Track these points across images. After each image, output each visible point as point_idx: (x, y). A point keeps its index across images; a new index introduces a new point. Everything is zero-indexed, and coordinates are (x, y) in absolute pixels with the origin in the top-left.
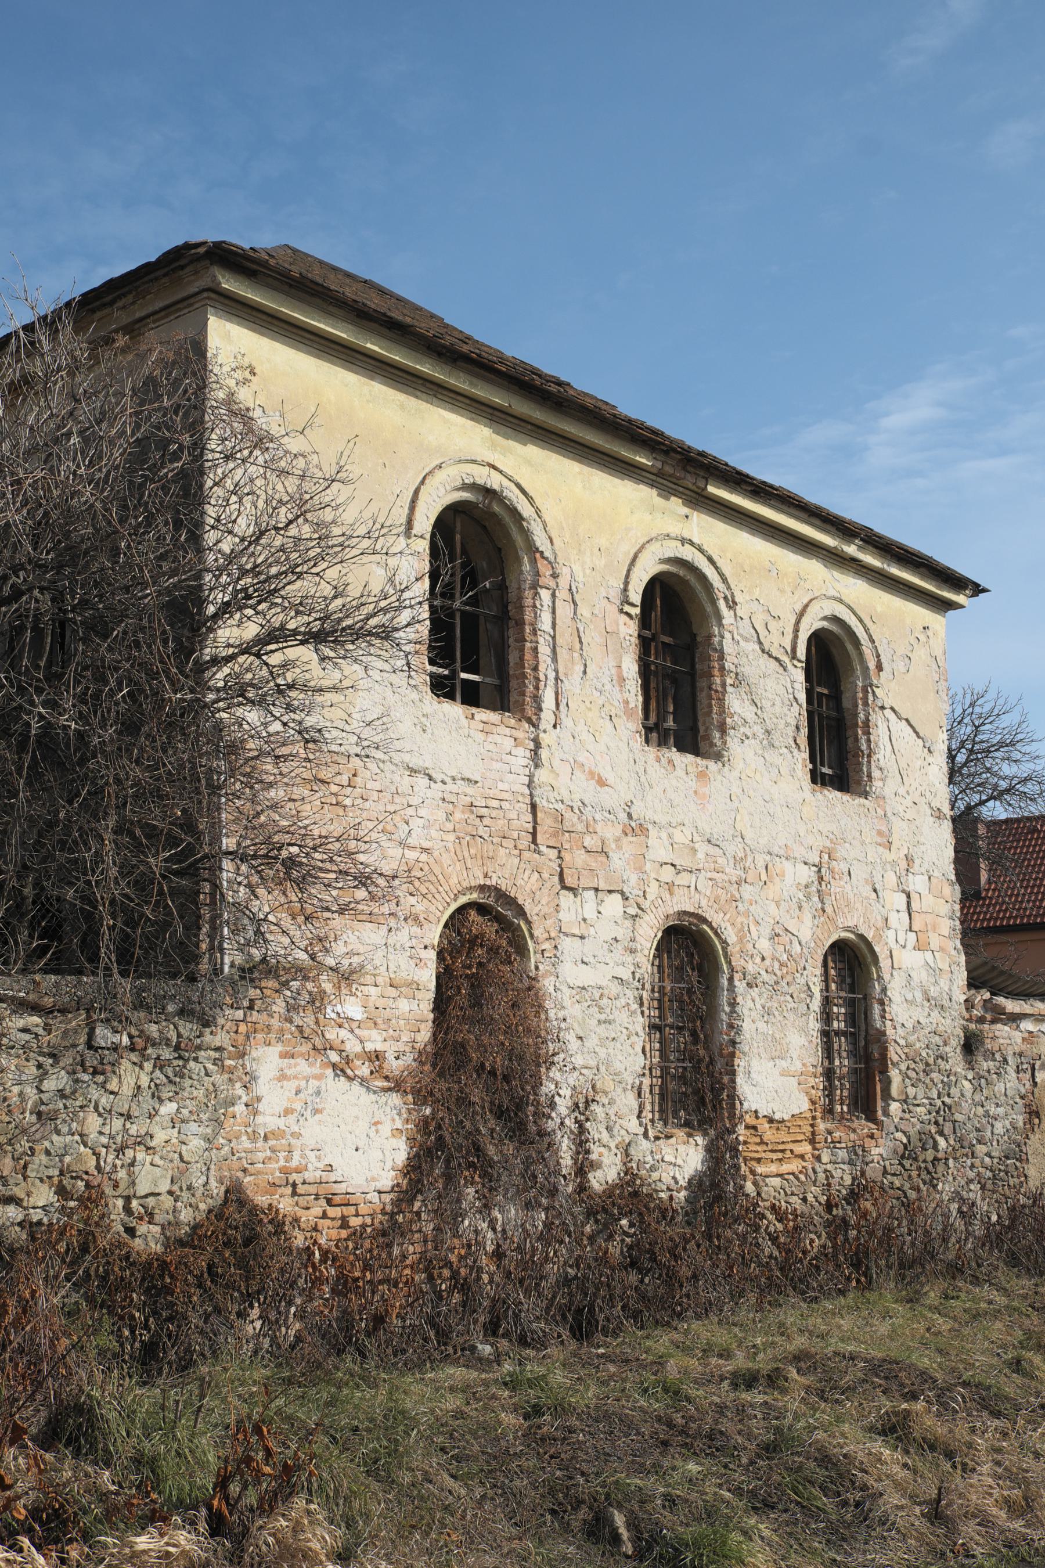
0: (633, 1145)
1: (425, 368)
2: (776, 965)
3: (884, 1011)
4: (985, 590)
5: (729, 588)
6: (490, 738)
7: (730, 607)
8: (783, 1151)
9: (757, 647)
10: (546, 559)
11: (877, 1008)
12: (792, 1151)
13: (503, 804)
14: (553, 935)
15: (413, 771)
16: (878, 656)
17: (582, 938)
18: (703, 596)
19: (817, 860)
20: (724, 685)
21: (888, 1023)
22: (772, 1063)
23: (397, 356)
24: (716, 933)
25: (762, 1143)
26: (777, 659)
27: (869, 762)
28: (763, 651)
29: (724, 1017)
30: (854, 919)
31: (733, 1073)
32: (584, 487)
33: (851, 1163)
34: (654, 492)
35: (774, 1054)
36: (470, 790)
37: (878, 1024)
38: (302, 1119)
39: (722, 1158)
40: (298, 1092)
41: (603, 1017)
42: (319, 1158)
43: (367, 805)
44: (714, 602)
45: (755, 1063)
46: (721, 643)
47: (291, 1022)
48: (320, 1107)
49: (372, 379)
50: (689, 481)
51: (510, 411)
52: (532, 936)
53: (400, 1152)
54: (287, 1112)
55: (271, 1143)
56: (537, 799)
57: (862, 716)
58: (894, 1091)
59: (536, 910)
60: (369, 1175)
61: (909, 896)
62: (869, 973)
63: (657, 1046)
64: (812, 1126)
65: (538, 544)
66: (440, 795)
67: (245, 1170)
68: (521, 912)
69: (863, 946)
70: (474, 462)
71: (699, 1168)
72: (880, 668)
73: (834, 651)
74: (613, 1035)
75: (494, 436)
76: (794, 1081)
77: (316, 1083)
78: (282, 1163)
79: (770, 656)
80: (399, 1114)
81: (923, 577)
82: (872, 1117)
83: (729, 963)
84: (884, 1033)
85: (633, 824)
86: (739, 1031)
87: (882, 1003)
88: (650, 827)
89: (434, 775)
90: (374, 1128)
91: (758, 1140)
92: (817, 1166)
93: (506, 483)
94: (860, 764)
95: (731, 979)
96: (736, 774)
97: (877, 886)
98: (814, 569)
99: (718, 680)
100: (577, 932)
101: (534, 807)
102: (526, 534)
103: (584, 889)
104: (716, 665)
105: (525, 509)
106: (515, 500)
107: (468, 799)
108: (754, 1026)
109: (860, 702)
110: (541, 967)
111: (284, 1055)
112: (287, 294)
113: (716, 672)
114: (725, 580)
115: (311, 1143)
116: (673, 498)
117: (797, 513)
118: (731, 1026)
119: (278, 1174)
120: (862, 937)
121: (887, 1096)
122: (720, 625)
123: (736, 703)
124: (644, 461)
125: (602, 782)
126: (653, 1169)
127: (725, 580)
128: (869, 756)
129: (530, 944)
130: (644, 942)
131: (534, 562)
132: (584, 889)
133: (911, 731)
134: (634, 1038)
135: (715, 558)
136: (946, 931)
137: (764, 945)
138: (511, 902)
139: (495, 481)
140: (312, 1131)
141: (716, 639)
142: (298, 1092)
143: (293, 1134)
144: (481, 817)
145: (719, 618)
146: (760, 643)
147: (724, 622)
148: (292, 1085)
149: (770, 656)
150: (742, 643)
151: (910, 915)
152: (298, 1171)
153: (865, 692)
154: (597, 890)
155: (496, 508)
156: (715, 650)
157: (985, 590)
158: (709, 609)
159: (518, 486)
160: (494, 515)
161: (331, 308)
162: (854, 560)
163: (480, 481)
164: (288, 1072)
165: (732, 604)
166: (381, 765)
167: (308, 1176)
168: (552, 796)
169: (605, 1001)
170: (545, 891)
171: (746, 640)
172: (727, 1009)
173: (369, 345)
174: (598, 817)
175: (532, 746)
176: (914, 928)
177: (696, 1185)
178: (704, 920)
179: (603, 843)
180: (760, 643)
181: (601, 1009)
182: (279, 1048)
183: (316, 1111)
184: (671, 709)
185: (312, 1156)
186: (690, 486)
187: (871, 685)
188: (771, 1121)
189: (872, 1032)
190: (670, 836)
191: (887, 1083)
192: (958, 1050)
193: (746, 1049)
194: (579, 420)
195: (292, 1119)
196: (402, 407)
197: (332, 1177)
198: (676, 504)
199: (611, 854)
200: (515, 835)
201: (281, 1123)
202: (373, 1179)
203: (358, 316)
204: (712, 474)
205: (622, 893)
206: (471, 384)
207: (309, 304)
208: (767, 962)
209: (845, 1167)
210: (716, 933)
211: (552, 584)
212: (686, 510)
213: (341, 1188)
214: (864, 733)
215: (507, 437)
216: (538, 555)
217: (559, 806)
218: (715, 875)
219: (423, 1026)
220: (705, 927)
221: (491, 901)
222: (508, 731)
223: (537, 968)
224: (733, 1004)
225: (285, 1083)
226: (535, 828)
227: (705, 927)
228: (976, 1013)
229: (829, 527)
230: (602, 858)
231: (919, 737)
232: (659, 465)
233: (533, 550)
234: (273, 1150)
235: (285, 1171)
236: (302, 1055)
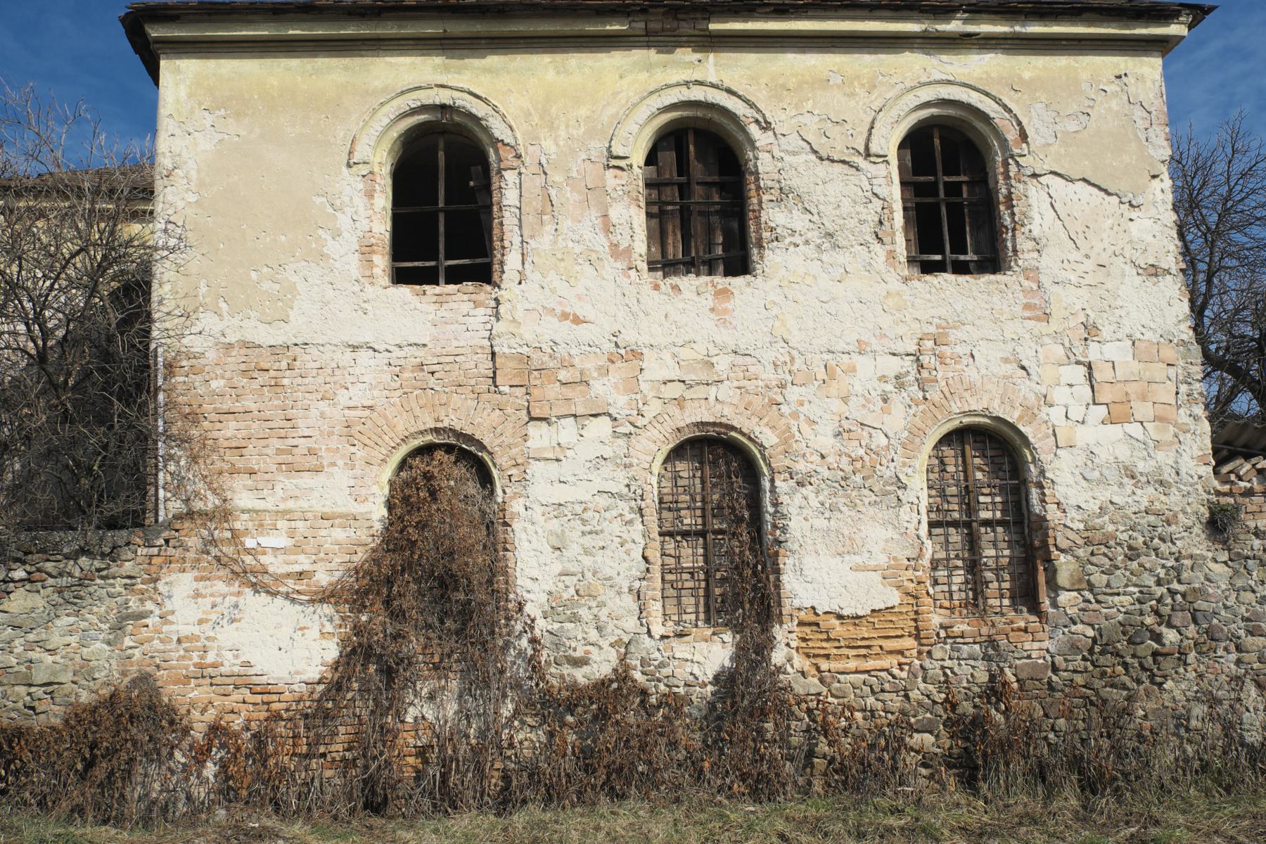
0: (633, 643)
1: (349, 31)
2: (845, 460)
3: (1044, 494)
4: (1212, 9)
5: (759, 111)
6: (445, 306)
7: (764, 129)
8: (868, 647)
9: (813, 157)
10: (508, 145)
11: (1034, 492)
12: (881, 647)
13: (457, 359)
14: (520, 461)
15: (355, 348)
16: (1019, 123)
17: (558, 460)
18: (732, 127)
19: (912, 348)
20: (760, 202)
21: (1052, 508)
22: (839, 559)
23: (320, 31)
24: (750, 438)
25: (828, 640)
26: (843, 162)
27: (1014, 236)
28: (821, 159)
29: (768, 518)
30: (988, 399)
31: (778, 572)
32: (558, 73)
33: (987, 658)
34: (652, 52)
35: (841, 549)
36: (420, 353)
37: (1037, 509)
38: (217, 628)
39: (753, 652)
40: (214, 606)
41: (588, 528)
42: (236, 657)
43: (306, 381)
44: (743, 129)
45: (809, 561)
46: (756, 166)
47: (208, 553)
48: (238, 617)
49: (316, 56)
50: (685, 28)
51: (447, 35)
52: (495, 465)
53: (332, 651)
54: (200, 622)
55: (184, 645)
56: (496, 349)
57: (1004, 191)
58: (1063, 578)
59: (497, 441)
60: (293, 670)
61: (1089, 367)
62: (1023, 456)
63: (701, 551)
64: (915, 620)
65: (497, 134)
66: (386, 361)
67: (158, 667)
68: (482, 447)
69: (1005, 429)
70: (419, 88)
71: (727, 663)
72: (1024, 136)
73: (971, 136)
74: (602, 544)
75: (448, 61)
76: (876, 577)
77: (234, 599)
78: (196, 660)
79: (833, 161)
80: (331, 620)
81: (1090, 23)
82: (1035, 608)
83: (769, 465)
84: (1044, 519)
85: (623, 352)
86: (784, 529)
87: (1040, 486)
88: (645, 351)
89: (376, 347)
90: (300, 633)
91: (824, 636)
92: (927, 663)
93: (456, 94)
94: (1005, 240)
95: (772, 481)
96: (775, 282)
97: (1025, 363)
98: (913, 64)
99: (755, 201)
100: (551, 456)
101: (493, 354)
102: (486, 130)
103: (559, 417)
104: (753, 186)
105: (478, 109)
106: (468, 106)
107: (418, 360)
108: (806, 525)
109: (1000, 178)
110: (507, 490)
111: (196, 579)
112: (210, 21)
113: (753, 193)
114: (751, 105)
115: (229, 645)
116: (678, 50)
117: (851, 13)
118: (775, 526)
119: (192, 668)
120: (998, 419)
121: (1054, 587)
122: (754, 148)
123: (774, 215)
124: (617, 27)
125: (577, 320)
126: (662, 665)
127: (751, 105)
128: (1014, 230)
129: (495, 472)
130: (642, 457)
131: (497, 151)
132: (559, 417)
133: (1095, 190)
134: (629, 546)
135: (734, 88)
136: (1165, 394)
137: (826, 441)
138: (470, 439)
139: (444, 97)
140: (227, 636)
141: (751, 164)
142: (214, 606)
143: (208, 638)
144: (433, 373)
145: (752, 142)
146: (815, 152)
147: (757, 144)
148: (208, 601)
149: (833, 161)
150: (787, 158)
151: (1092, 387)
152: (215, 666)
153: (1006, 164)
154: (575, 416)
155: (457, 118)
156: (752, 173)
157: (1212, 9)
158: (741, 137)
159: (471, 93)
160: (458, 125)
161: (249, 17)
162: (969, 35)
163: (430, 102)
164: (204, 592)
165: (766, 126)
166: (321, 348)
167: (223, 670)
168: (513, 342)
169: (590, 514)
170: (509, 425)
171: (794, 153)
172: (771, 510)
173: (291, 32)
174: (573, 352)
175: (493, 304)
176: (1099, 399)
177: (726, 681)
178: (733, 428)
179: (581, 374)
180: (815, 152)
181: (584, 522)
182: (196, 573)
183: (233, 621)
184: (720, 240)
185: (229, 655)
186: (692, 32)
187: (1012, 157)
188: (840, 617)
189: (1033, 518)
190: (674, 355)
191: (1052, 573)
192: (1197, 529)
193: (796, 547)
194: (528, 17)
195: (205, 627)
196: (346, 68)
197: (251, 671)
198: (685, 55)
199: (591, 382)
200: (473, 382)
201: (196, 630)
202: (297, 673)
203: (274, 14)
204: (712, 13)
205: (610, 415)
206: (400, 27)
207: (230, 21)
208: (830, 459)
209: (979, 663)
210: (750, 438)
211: (516, 163)
212: (698, 56)
213: (264, 680)
214: (1007, 209)
215: (462, 57)
216: (500, 144)
217: (525, 350)
218: (745, 383)
219: (359, 549)
220: (733, 434)
221: (453, 441)
222: (466, 297)
223: (504, 492)
224: (776, 504)
225: (200, 600)
226: (494, 373)
227: (733, 434)
228: (399, 511)
229: (905, 13)
230: (583, 387)
231: (1109, 194)
232: (642, 25)
233: (496, 142)
234: (186, 650)
235: (200, 666)
236: (220, 578)
